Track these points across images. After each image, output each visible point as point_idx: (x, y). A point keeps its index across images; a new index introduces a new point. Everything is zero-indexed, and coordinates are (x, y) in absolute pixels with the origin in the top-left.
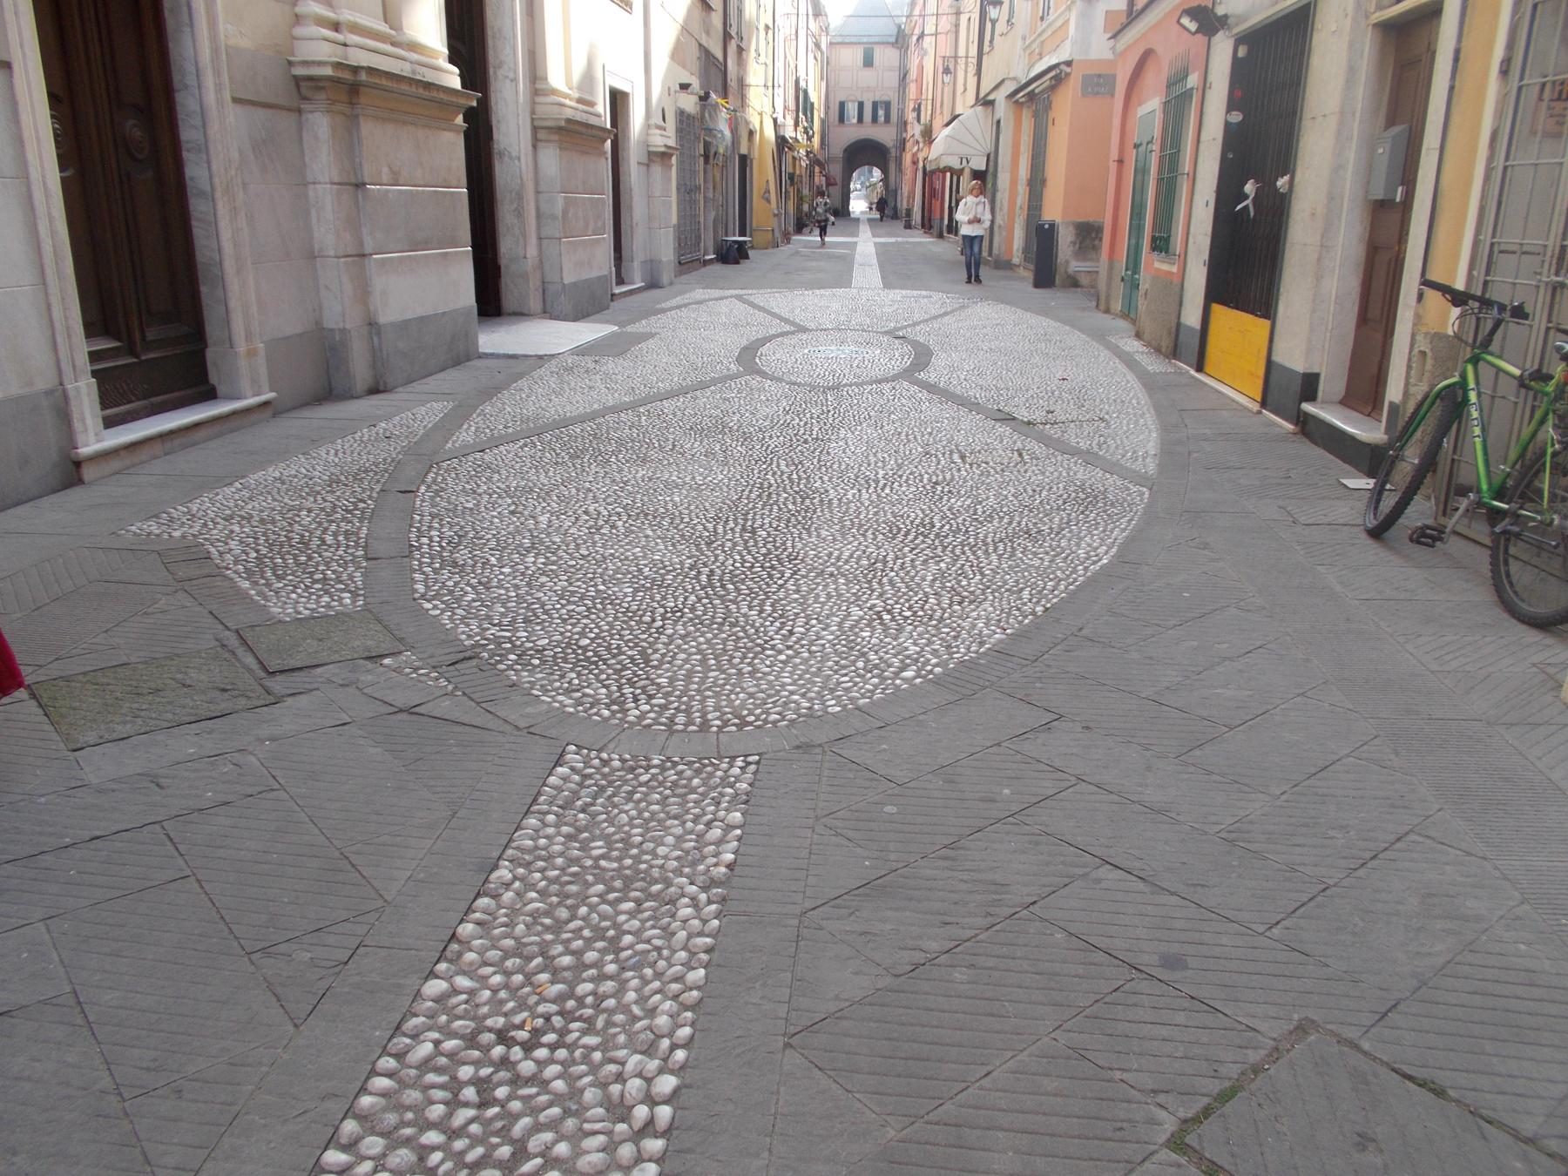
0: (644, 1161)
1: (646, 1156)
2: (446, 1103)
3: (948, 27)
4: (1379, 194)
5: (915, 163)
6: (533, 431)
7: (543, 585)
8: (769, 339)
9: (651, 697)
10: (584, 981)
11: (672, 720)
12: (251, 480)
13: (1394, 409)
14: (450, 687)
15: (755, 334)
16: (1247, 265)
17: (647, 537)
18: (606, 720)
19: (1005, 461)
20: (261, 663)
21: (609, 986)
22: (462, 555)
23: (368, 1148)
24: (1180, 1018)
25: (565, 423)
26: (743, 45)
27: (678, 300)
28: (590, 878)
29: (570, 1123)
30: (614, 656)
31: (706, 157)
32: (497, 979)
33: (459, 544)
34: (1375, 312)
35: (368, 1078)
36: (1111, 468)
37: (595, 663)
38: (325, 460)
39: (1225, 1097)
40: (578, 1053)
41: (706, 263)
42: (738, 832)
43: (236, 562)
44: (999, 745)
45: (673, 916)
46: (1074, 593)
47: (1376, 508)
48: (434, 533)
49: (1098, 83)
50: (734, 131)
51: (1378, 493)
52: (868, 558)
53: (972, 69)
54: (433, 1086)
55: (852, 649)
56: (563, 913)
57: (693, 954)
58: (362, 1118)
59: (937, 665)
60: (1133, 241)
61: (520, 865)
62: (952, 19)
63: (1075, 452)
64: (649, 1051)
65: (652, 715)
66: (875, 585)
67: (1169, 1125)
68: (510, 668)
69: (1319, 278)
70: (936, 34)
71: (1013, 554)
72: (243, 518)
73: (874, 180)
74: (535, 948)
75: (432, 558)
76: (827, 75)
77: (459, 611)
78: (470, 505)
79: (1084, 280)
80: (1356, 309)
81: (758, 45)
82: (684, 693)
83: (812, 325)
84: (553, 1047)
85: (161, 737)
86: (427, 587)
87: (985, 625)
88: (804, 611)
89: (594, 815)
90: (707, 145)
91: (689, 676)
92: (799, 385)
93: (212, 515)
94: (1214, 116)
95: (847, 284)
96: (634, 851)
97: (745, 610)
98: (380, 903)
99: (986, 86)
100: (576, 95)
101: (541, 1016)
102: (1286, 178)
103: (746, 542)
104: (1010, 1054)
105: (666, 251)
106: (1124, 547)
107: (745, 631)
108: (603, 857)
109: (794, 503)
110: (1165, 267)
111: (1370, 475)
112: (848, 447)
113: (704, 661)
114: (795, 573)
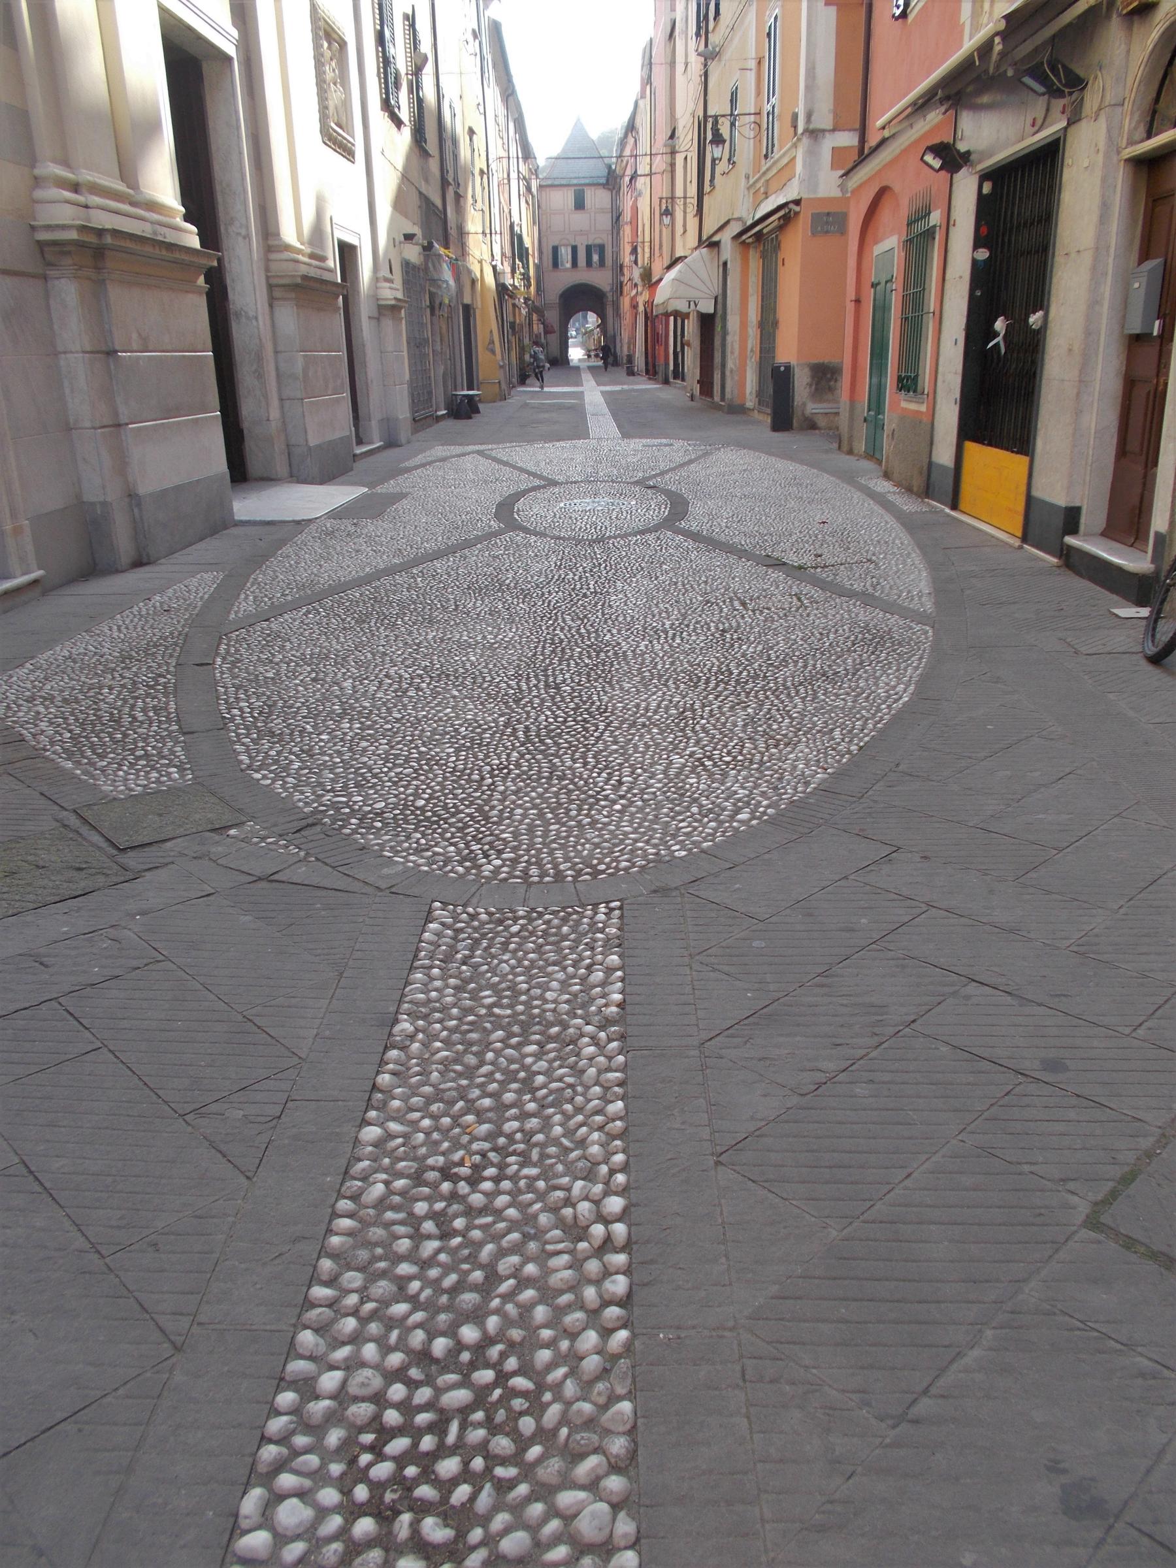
0: (611, 1274)
1: (612, 1270)
2: (410, 1237)
3: (663, 166)
4: (1136, 328)
5: (635, 306)
6: (313, 597)
7: (365, 750)
8: (524, 493)
9: (500, 852)
10: (509, 1120)
11: (525, 872)
12: (42, 659)
13: (1160, 538)
14: (302, 854)
15: (507, 490)
16: (1000, 401)
17: (454, 697)
18: (461, 876)
19: (786, 606)
20: (108, 840)
21: (534, 1123)
22: (277, 724)
23: (349, 1282)
24: (1072, 1114)
25: (341, 588)
26: (461, 192)
27: (419, 459)
28: (488, 1025)
29: (532, 1246)
30: (453, 815)
31: (432, 308)
32: (426, 1122)
33: (270, 713)
34: (1134, 444)
35: (330, 1222)
36: (889, 608)
37: (436, 822)
38: (111, 636)
39: (1128, 1179)
40: (522, 1183)
41: (438, 419)
42: (619, 973)
43: (52, 743)
44: (846, 878)
45: (578, 1055)
46: (881, 731)
47: (1153, 636)
48: (242, 704)
49: (829, 221)
50: (458, 279)
51: (1155, 619)
52: (676, 706)
53: (692, 210)
54: (394, 1223)
55: (682, 795)
56: (471, 1060)
57: (606, 1089)
58: (334, 1256)
59: (768, 807)
60: (875, 380)
61: (419, 1018)
62: (667, 158)
63: (851, 594)
64: (589, 1176)
65: (505, 869)
66: (690, 734)
67: (1083, 1209)
68: (355, 832)
69: (1078, 413)
70: (650, 175)
71: (815, 697)
72: (45, 699)
73: (590, 326)
74: (454, 1093)
75: (247, 728)
76: (539, 219)
77: (290, 780)
78: (270, 675)
79: (822, 422)
80: (1115, 441)
81: (475, 188)
82: (531, 846)
83: (561, 479)
84: (497, 1180)
85: (29, 918)
86: (250, 757)
87: (804, 766)
88: (627, 760)
89: (476, 967)
90: (432, 296)
91: (531, 830)
92: (563, 539)
93: (13, 697)
94: (961, 252)
95: (585, 435)
96: (523, 998)
97: (569, 763)
98: (296, 1060)
99: (709, 227)
100: (309, 251)
101: (477, 1153)
102: (1040, 314)
103: (553, 698)
104: (923, 1157)
105: (402, 411)
106: (923, 682)
107: (575, 784)
108: (494, 1005)
109: (589, 657)
110: (913, 406)
111: (1141, 604)
112: (627, 599)
113: (541, 815)
114: (608, 725)
